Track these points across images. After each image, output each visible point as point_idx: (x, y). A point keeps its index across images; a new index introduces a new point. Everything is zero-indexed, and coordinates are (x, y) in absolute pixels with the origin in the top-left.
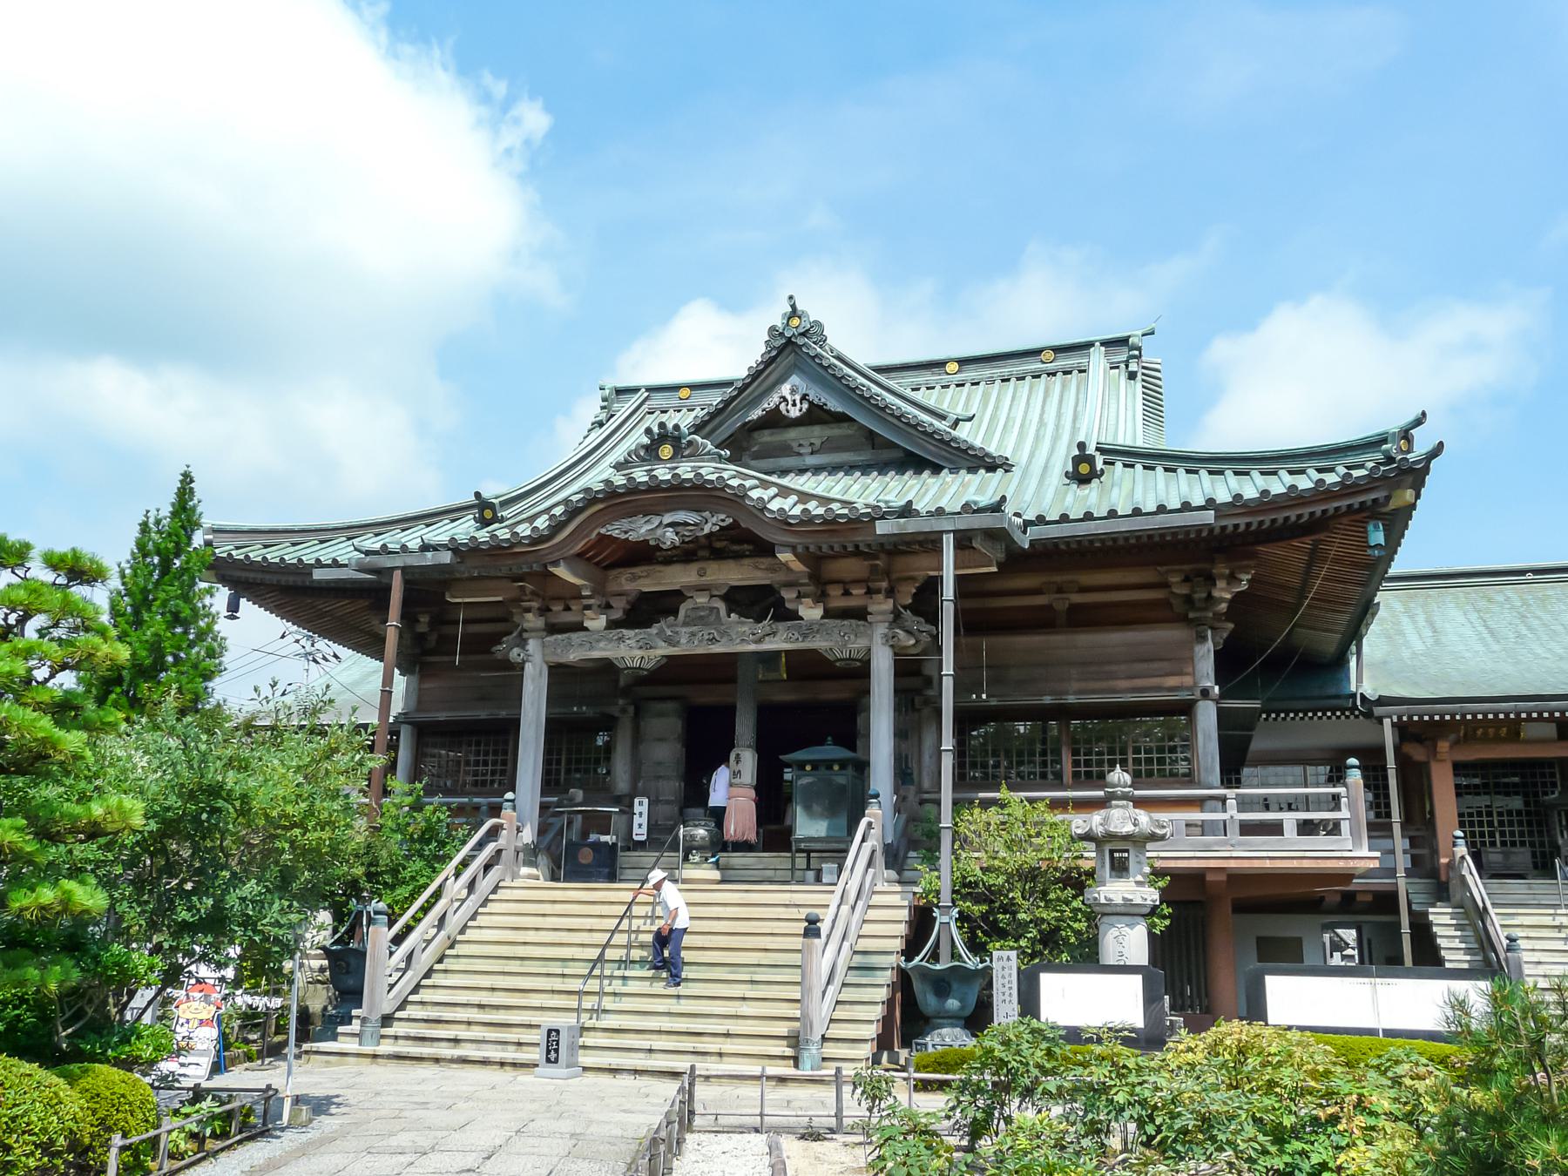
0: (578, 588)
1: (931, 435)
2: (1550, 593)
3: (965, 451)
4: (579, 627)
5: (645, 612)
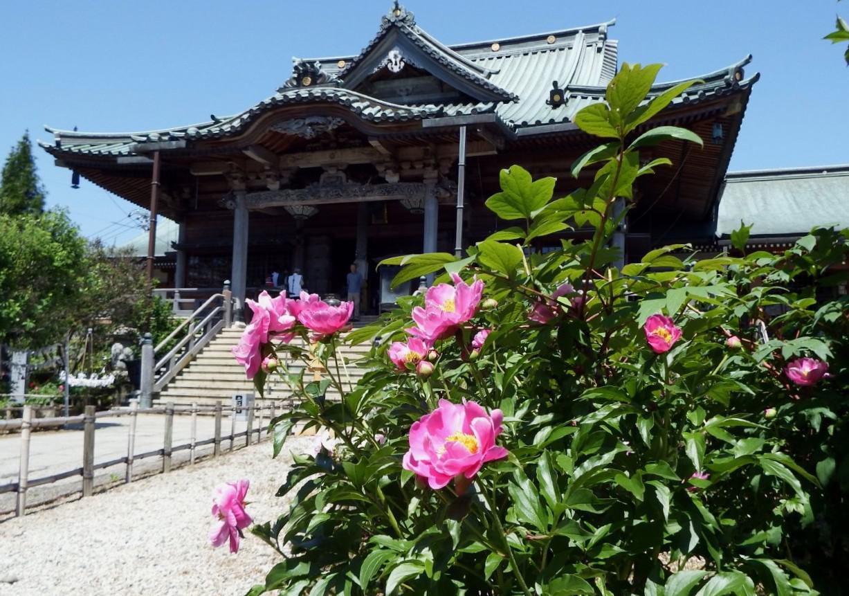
0: (262, 165)
1: (475, 81)
2: (835, 182)
3: (492, 91)
4: (264, 189)
5: (303, 179)
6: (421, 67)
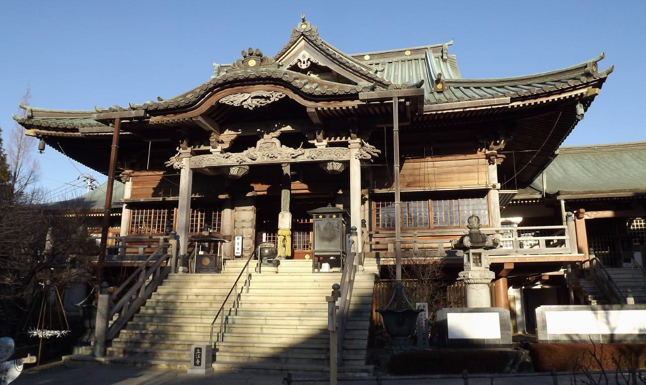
6: (324, 65)
